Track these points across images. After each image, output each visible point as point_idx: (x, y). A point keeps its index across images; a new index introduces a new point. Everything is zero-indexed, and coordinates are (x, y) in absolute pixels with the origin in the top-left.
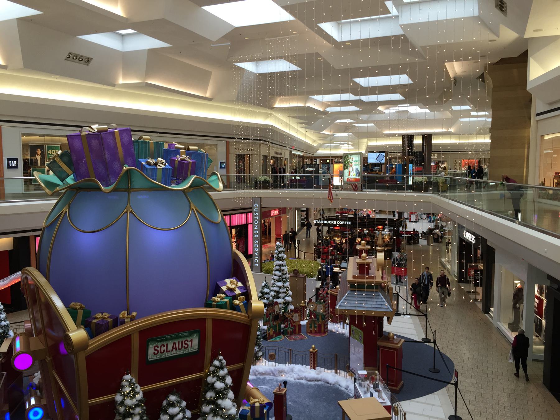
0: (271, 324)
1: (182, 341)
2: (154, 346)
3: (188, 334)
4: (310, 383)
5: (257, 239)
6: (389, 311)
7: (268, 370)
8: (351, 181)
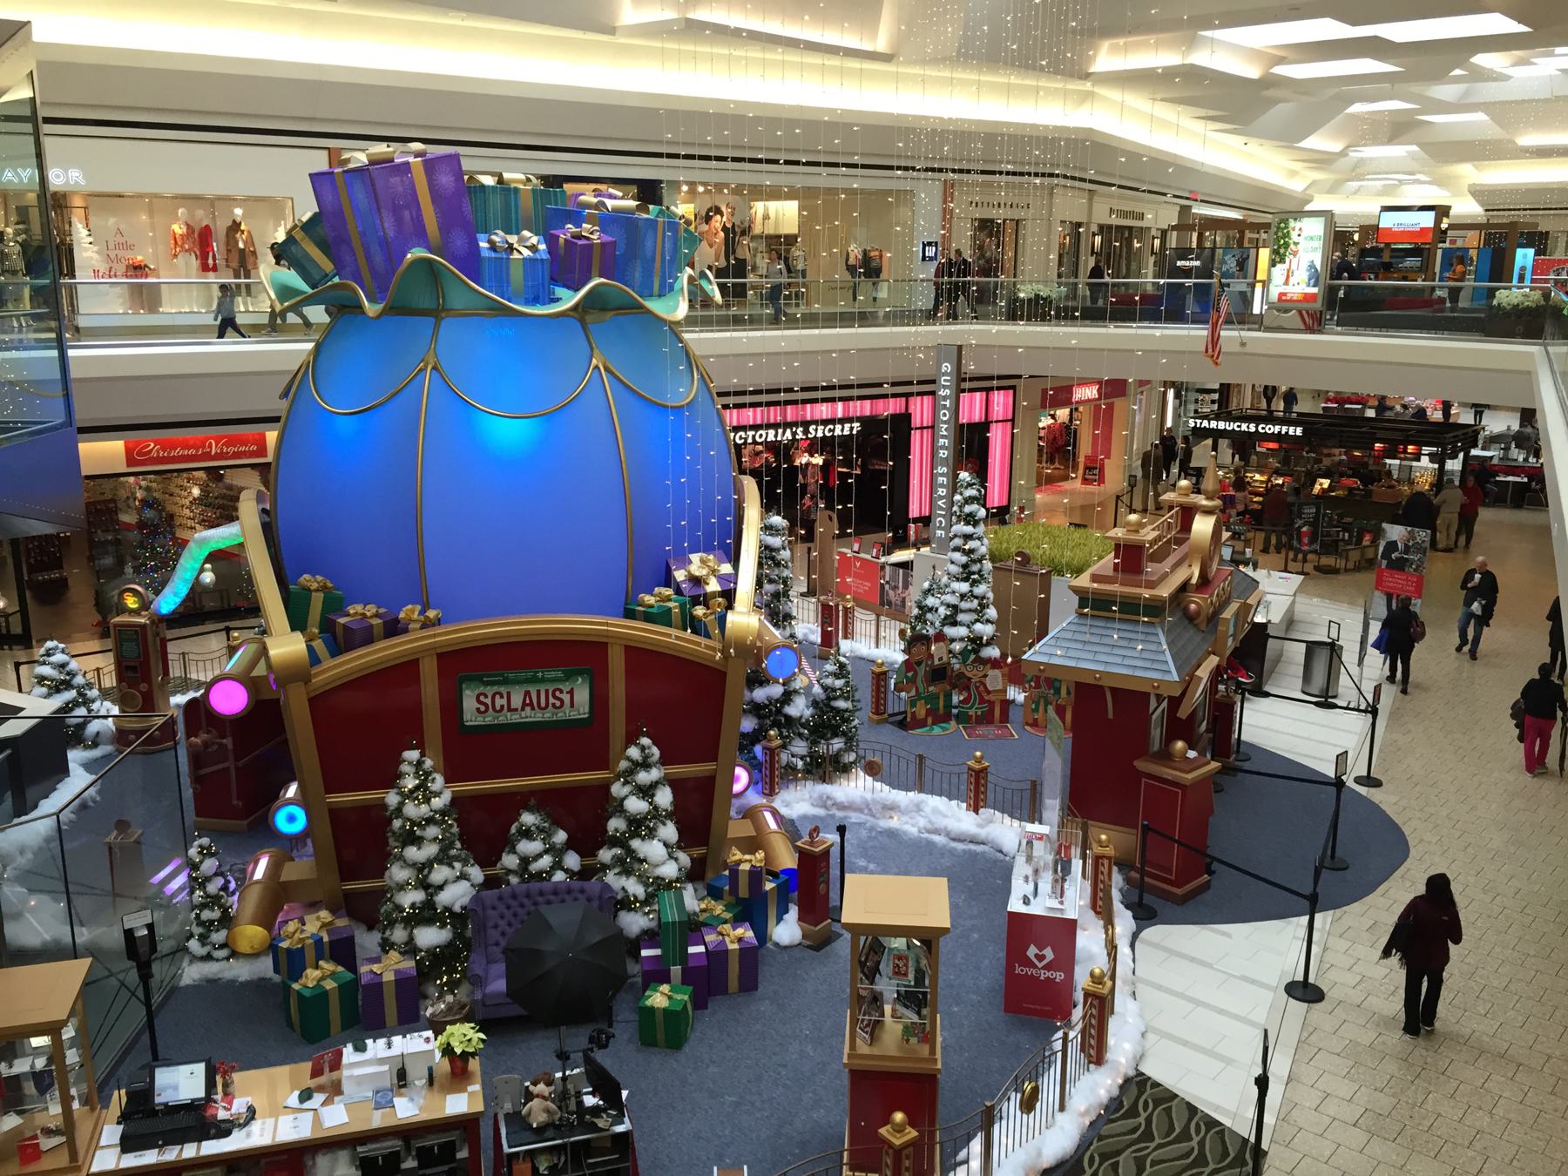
0: (921, 690)
1: (547, 691)
2: (477, 692)
3: (560, 674)
4: (954, 844)
5: (944, 462)
6: (1167, 678)
7: (858, 800)
8: (1291, 301)
